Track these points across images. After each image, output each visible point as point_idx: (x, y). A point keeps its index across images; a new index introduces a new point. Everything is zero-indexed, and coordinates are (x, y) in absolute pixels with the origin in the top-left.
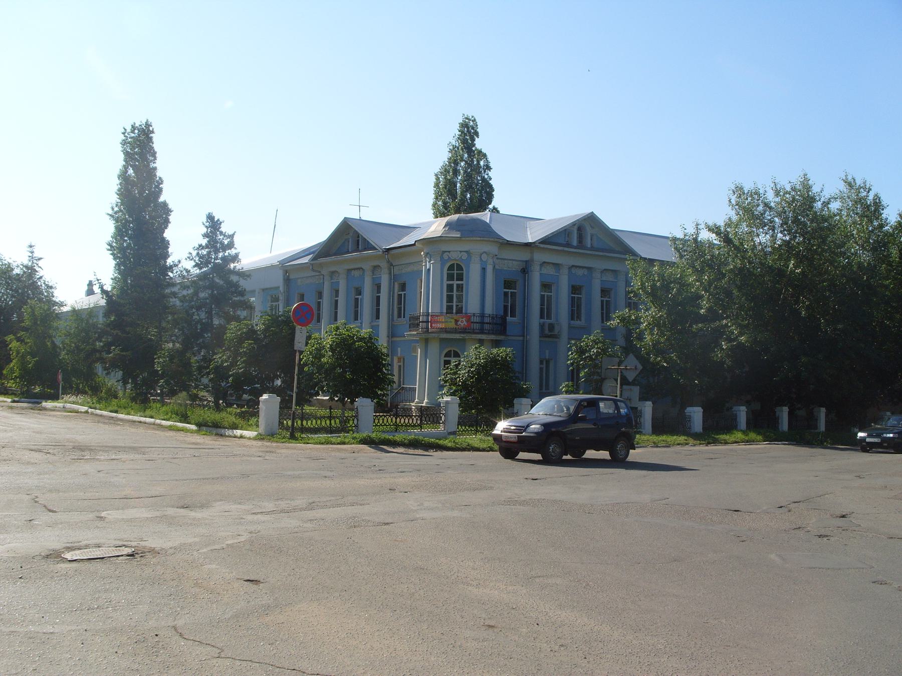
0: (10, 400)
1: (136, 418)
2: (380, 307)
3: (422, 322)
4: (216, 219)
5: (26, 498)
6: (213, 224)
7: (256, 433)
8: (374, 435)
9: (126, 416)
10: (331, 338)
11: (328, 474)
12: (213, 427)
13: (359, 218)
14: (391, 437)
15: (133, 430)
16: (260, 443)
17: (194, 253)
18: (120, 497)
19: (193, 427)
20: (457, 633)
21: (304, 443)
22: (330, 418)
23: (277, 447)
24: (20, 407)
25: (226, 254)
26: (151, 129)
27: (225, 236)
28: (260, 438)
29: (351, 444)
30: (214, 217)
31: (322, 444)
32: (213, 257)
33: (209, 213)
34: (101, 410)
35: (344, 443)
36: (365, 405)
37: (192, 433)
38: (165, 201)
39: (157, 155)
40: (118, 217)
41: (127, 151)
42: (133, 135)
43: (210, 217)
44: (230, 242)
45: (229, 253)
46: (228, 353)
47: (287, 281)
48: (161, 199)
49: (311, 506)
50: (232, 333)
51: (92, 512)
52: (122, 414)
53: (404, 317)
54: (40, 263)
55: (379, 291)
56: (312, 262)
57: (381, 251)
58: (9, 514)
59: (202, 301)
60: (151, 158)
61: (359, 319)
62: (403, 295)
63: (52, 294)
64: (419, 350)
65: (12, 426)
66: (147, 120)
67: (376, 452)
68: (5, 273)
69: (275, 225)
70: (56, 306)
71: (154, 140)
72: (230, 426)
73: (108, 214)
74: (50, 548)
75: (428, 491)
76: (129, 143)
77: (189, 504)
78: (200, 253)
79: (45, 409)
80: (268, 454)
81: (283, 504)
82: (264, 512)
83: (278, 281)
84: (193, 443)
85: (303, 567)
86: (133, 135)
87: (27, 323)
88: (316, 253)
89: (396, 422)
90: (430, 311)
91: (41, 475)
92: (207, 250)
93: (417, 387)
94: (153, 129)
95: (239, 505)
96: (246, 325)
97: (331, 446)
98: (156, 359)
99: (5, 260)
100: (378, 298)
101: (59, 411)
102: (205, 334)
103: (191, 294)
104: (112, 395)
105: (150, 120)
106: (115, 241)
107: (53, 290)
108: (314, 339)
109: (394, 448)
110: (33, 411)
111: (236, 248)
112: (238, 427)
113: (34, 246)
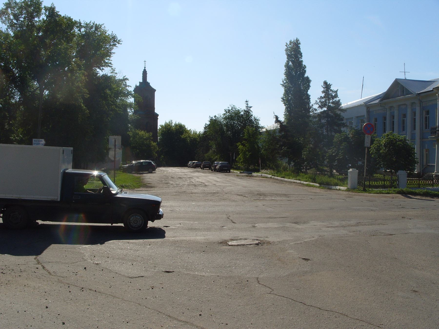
0: (239, 172)
1: (292, 180)
2: (416, 124)
3: (438, 131)
4: (328, 84)
5: (225, 216)
6: (327, 86)
7: (346, 188)
8: (404, 189)
9: (288, 179)
10: (385, 140)
11: (375, 208)
12: (327, 185)
13: (405, 79)
14: (413, 190)
15: (289, 186)
16: (347, 193)
17: (318, 101)
18: (267, 217)
19: (318, 185)
20: (394, 293)
21: (369, 193)
22: (384, 180)
23: (354, 195)
24: (242, 175)
25: (334, 100)
26: (299, 42)
27: (333, 91)
28: (348, 190)
29: (393, 194)
30: (327, 83)
31: (378, 193)
32: (328, 102)
33: (325, 81)
34: (277, 177)
35: (389, 193)
36: (402, 174)
37: (316, 187)
38: (308, 76)
39: (302, 55)
40: (286, 85)
41: (288, 54)
42: (290, 46)
43: (325, 83)
44: (336, 94)
45: (335, 100)
46: (335, 149)
47: (368, 112)
48: (306, 76)
49: (358, 224)
50: (337, 139)
51: (251, 224)
52: (286, 178)
53: (429, 129)
54: (251, 109)
55: (415, 115)
56: (381, 102)
57: (415, 95)
58: (215, 223)
59: (323, 124)
60: (300, 56)
61: (405, 130)
62: (428, 117)
63: (258, 123)
64: (436, 145)
65: (235, 184)
66: (297, 38)
67: (405, 198)
68: (237, 114)
69: (363, 85)
70: (260, 128)
71: (301, 47)
72: (334, 185)
73: (281, 84)
74: (224, 239)
75: (422, 219)
76: (289, 50)
77: (298, 221)
78: (321, 100)
79: (253, 176)
80: (348, 198)
81: (344, 223)
82: (333, 227)
83: (364, 112)
84: (315, 193)
85: (334, 254)
86: (290, 46)
87: (246, 137)
88: (382, 97)
89: (419, 183)
90: (437, 125)
91: (237, 206)
92: (324, 99)
93: (435, 164)
94: (300, 42)
95: (322, 223)
96: (343, 135)
97: (382, 195)
98: (303, 152)
99: (237, 108)
100: (415, 119)
101: (259, 177)
102: (325, 140)
103: (317, 121)
104: (285, 169)
105: (298, 38)
106: (285, 97)
107: (258, 121)
108: (377, 141)
109: (415, 196)
110: (246, 177)
111: (338, 97)
112: (338, 185)
113: (248, 101)
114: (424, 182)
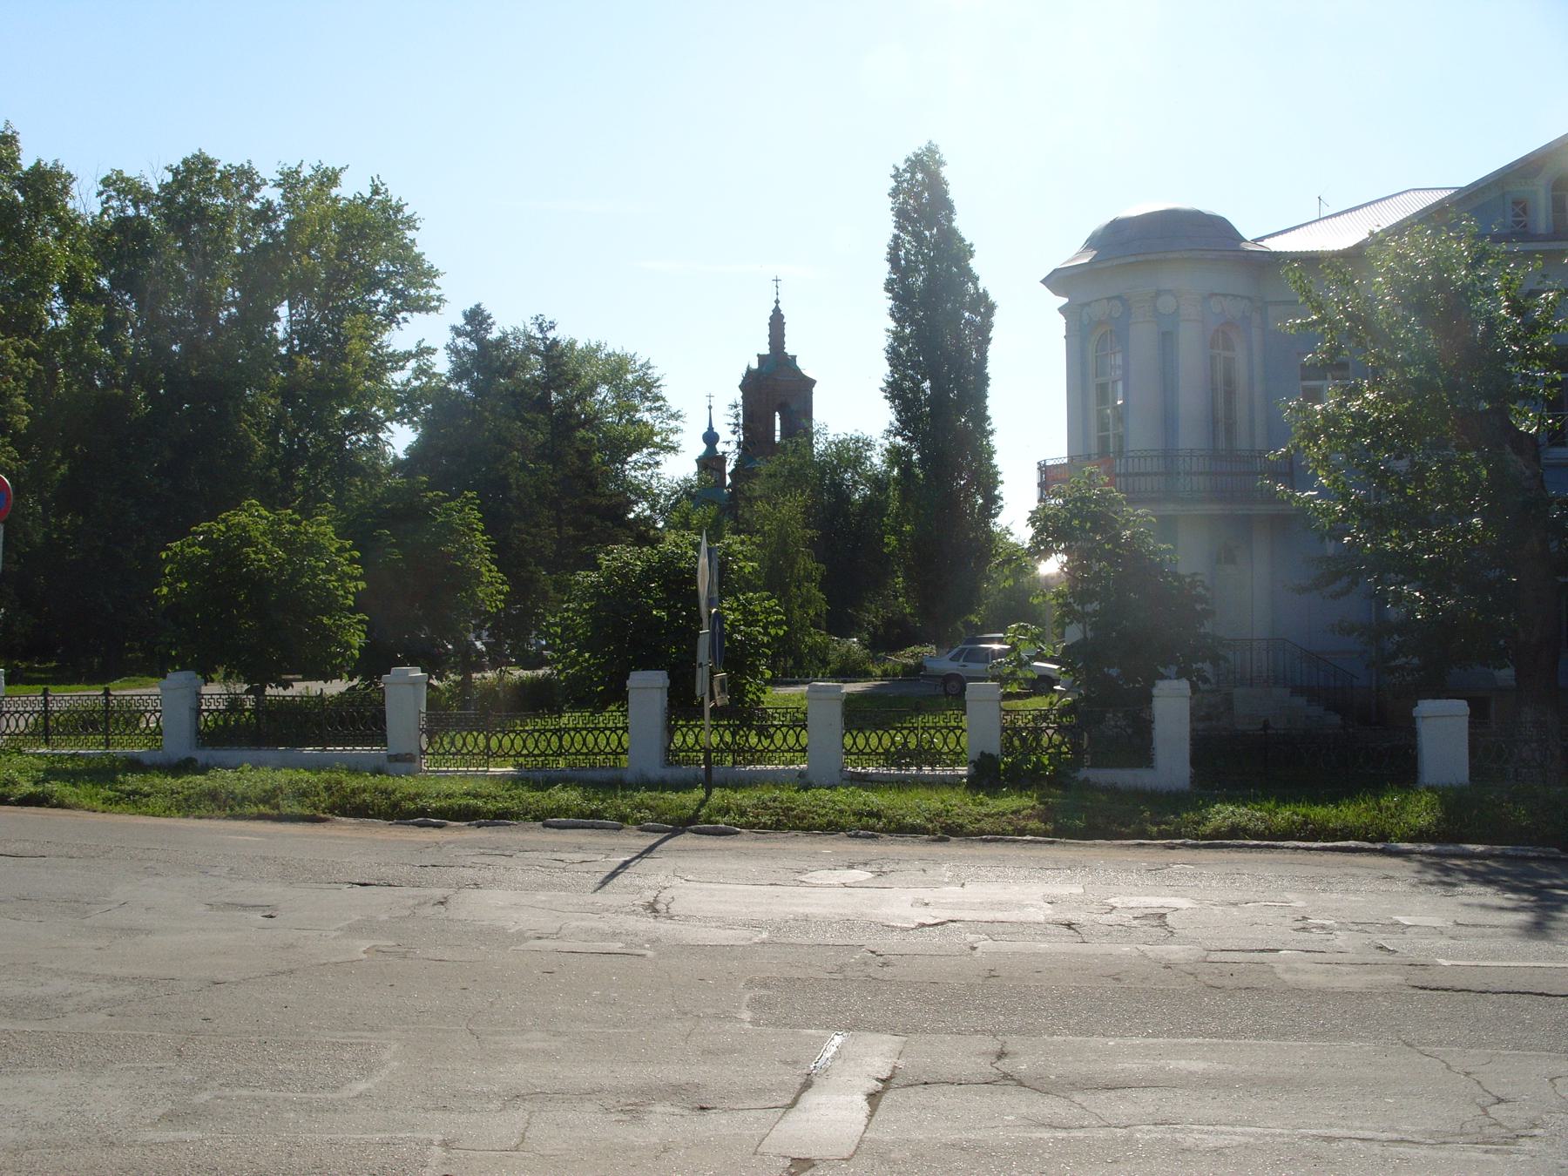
114: (476, 740)
